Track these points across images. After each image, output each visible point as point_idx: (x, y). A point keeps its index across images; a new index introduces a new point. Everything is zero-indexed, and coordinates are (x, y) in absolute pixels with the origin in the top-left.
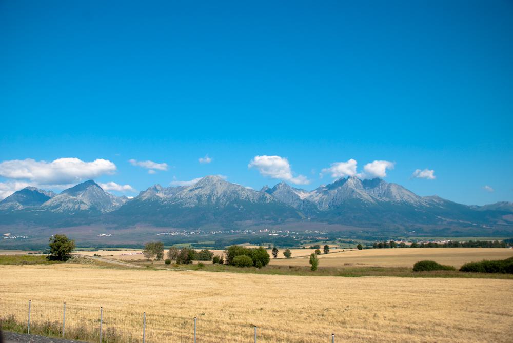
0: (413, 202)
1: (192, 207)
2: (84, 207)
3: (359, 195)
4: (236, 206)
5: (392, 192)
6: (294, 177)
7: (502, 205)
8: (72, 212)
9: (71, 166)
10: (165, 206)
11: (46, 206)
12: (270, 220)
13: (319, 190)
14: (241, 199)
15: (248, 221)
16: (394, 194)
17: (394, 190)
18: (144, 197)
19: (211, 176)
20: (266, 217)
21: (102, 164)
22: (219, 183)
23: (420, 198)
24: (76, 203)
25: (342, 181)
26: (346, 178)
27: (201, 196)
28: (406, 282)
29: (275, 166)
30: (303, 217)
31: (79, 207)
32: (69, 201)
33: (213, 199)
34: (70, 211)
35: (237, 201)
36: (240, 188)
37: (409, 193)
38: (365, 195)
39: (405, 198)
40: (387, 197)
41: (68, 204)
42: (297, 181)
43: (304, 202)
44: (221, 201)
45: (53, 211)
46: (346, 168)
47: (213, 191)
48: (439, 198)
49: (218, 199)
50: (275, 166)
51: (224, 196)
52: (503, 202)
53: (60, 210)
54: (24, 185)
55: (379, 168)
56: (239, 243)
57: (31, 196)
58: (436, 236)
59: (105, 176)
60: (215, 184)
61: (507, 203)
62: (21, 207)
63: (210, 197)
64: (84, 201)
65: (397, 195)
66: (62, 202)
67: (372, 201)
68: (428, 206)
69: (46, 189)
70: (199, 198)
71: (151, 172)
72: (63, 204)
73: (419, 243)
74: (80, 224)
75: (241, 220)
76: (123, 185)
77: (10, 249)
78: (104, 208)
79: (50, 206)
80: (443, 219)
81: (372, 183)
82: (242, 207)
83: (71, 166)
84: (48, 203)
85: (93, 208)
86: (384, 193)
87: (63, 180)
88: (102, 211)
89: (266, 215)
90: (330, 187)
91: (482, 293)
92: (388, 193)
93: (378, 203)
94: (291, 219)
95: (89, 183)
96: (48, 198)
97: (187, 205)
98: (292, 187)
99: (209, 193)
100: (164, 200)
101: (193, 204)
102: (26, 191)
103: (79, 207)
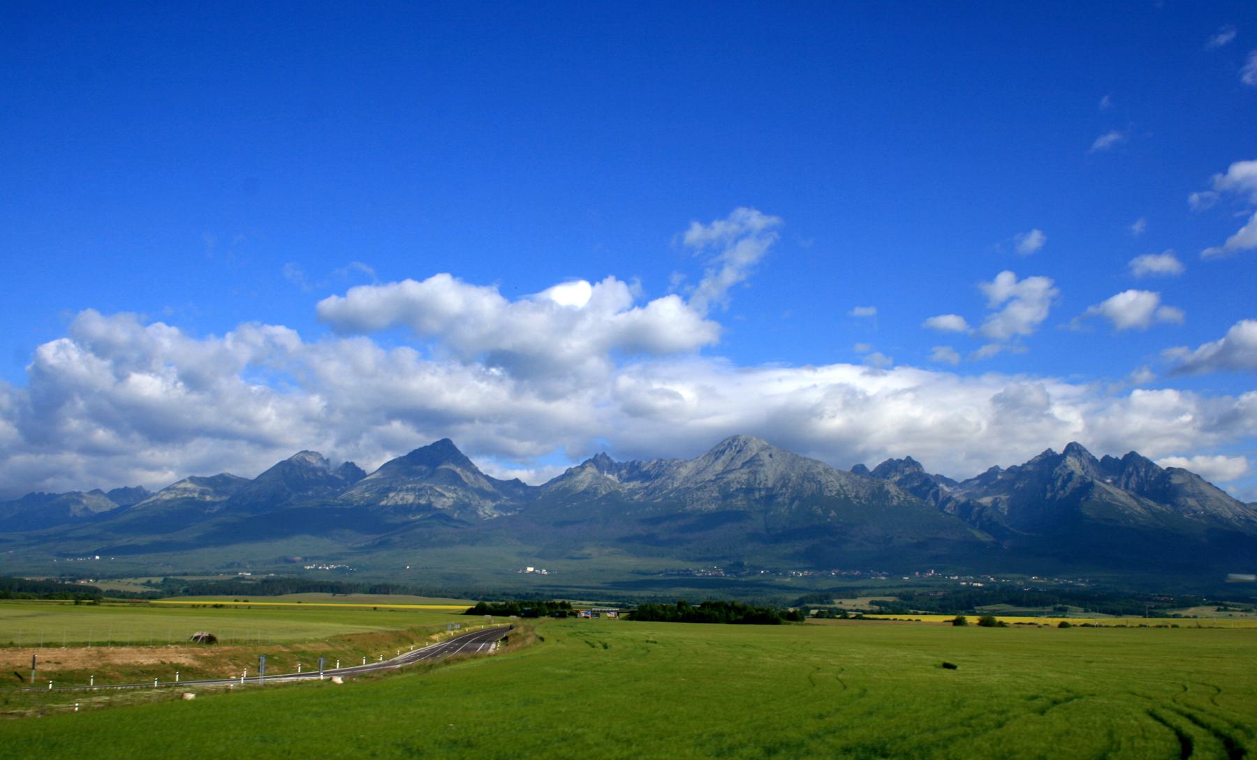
0: (1230, 515)
3: (1109, 493)
18: (582, 482)
82: (833, 513)
97: (697, 506)
101: (708, 502)
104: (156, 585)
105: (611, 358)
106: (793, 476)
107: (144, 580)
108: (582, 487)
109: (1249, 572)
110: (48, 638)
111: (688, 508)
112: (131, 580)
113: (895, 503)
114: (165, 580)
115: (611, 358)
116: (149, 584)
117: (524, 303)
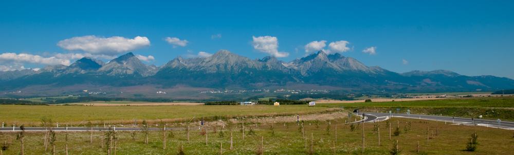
0: (364, 70)
2: (130, 72)
3: (331, 65)
4: (247, 72)
5: (350, 64)
6: (279, 50)
7: (415, 73)
9: (120, 44)
10: (192, 72)
11: (102, 71)
12: (275, 82)
13: (295, 61)
14: (249, 67)
15: (259, 83)
16: (351, 65)
17: (350, 61)
18: (174, 65)
19: (223, 51)
20: (272, 81)
21: (141, 40)
22: (231, 56)
23: (368, 67)
25: (313, 56)
26: (317, 53)
27: (219, 65)
29: (268, 44)
30: (298, 81)
31: (126, 72)
32: (118, 67)
34: (121, 75)
35: (246, 68)
36: (247, 59)
37: (361, 64)
38: (335, 65)
39: (360, 68)
40: (347, 66)
41: (118, 70)
42: (278, 55)
43: (290, 70)
44: (235, 69)
46: (316, 45)
47: (227, 61)
48: (379, 68)
50: (268, 44)
51: (236, 65)
52: (415, 71)
53: (113, 73)
54: (80, 56)
55: (340, 46)
56: (303, 98)
57: (87, 63)
58: (471, 92)
59: (142, 49)
60: (228, 56)
61: (418, 71)
62: (83, 72)
64: (128, 68)
65: (354, 65)
66: (113, 68)
67: (340, 69)
68: (375, 73)
69: (95, 58)
70: (218, 66)
71: (174, 47)
72: (114, 70)
73: (350, 97)
74: (134, 85)
75: (254, 83)
76: (18, 54)
77: (485, 91)
78: (143, 73)
80: (389, 82)
81: (336, 56)
82: (251, 73)
83: (120, 44)
84: (102, 69)
85: (136, 73)
86: (344, 64)
87: (110, 52)
88: (142, 75)
89: (272, 79)
90: (304, 60)
92: (347, 64)
93: (344, 71)
94: (290, 82)
95: (128, 56)
96: (101, 66)
97: (210, 72)
99: (224, 62)
100: (190, 68)
101: (214, 70)
102: (84, 60)
103: (126, 72)
104: (45, 100)
105: (487, 125)
106: (239, 62)
107: (40, 98)
108: (174, 67)
109: (479, 126)
110: (14, 116)
111: (207, 72)
112: (35, 98)
113: (270, 69)
114: (47, 98)
115: (487, 125)
116: (41, 99)
117: (182, 41)
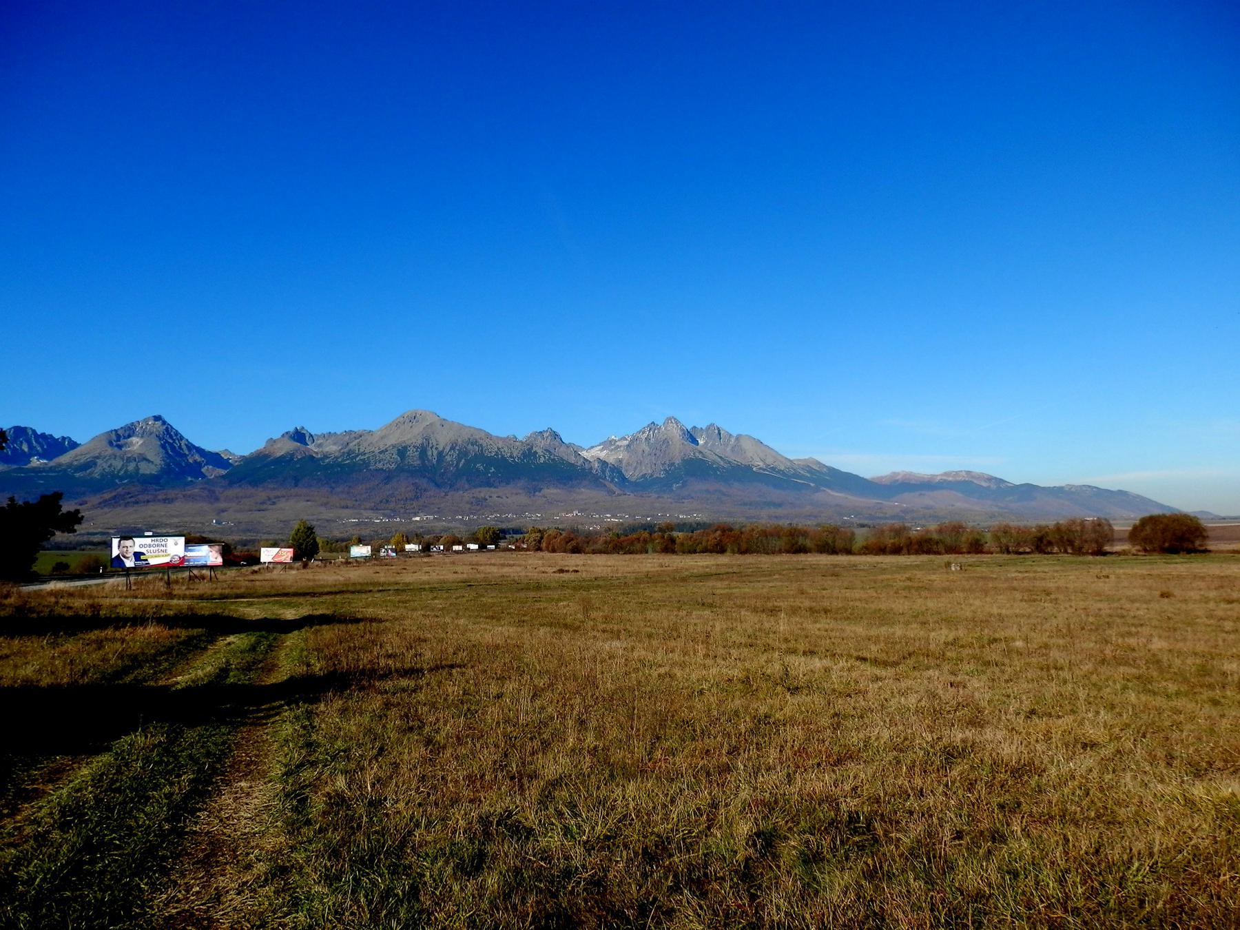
1: (390, 470)
8: (121, 479)
11: (60, 465)
17: (746, 445)
24: (129, 460)
28: (782, 563)
33: (429, 453)
35: (480, 457)
44: (448, 458)
45: (77, 475)
49: (440, 454)
51: (453, 448)
63: (423, 451)
66: (98, 458)
79: (70, 465)
84: (65, 459)
91: (1223, 605)
97: (380, 466)
98: (377, 451)
103: (137, 469)
